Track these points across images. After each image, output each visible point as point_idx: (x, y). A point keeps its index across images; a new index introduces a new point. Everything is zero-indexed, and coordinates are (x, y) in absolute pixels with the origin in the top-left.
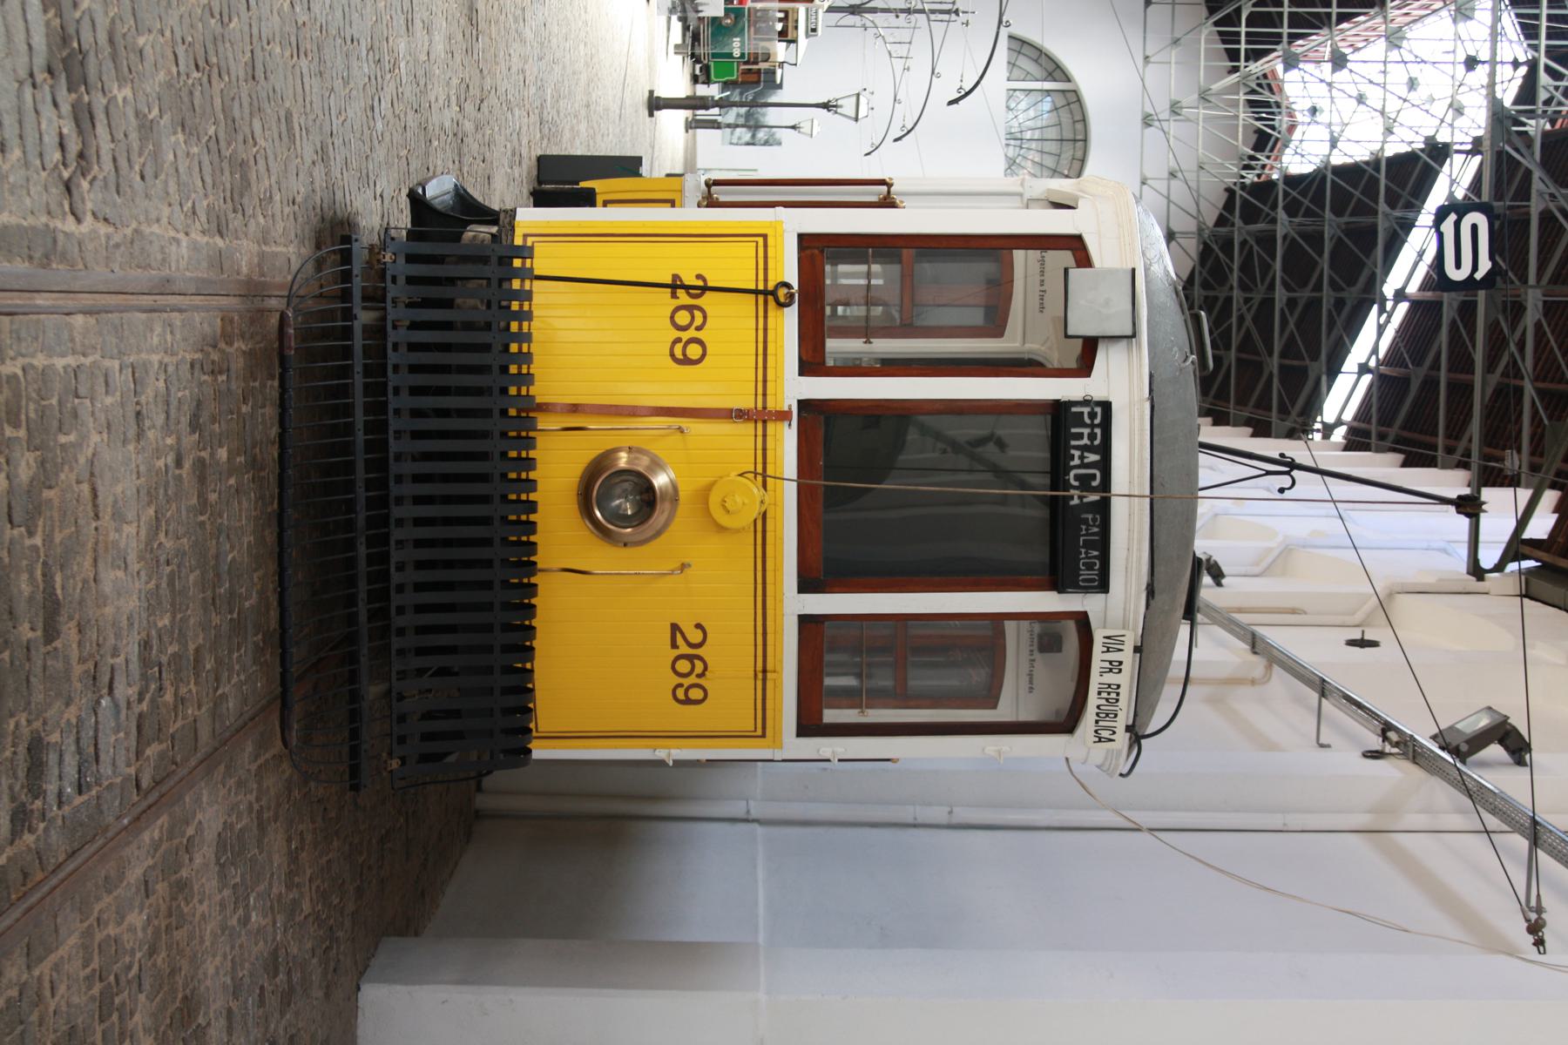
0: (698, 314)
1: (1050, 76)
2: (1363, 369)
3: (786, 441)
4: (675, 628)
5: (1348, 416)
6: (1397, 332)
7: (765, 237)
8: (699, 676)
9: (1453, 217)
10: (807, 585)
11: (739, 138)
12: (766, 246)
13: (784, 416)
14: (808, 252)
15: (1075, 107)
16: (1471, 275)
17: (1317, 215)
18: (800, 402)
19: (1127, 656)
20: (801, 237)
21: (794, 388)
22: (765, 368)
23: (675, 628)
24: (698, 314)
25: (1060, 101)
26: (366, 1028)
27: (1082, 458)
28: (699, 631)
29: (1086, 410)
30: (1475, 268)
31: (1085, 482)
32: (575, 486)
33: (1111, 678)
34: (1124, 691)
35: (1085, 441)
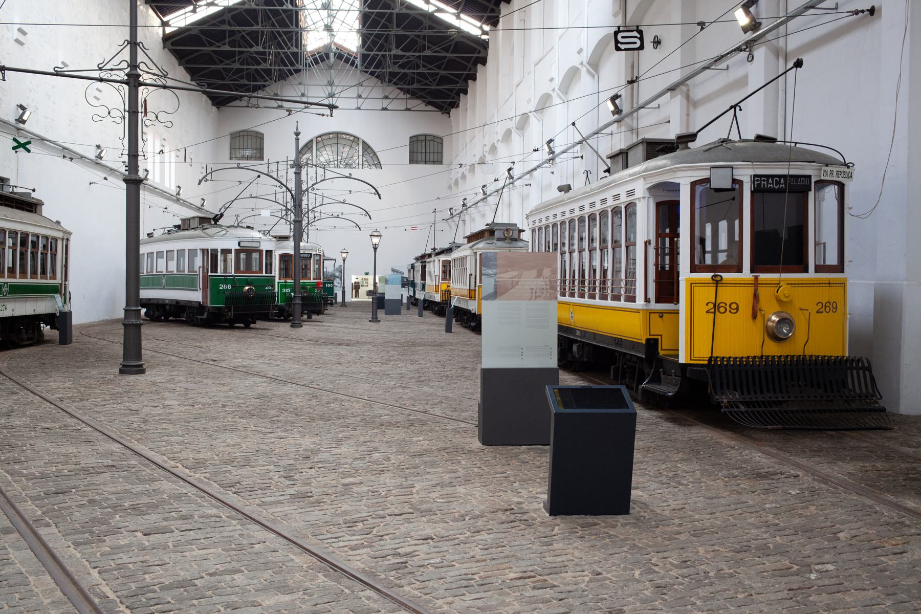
0: (721, 305)
1: (310, 149)
2: (458, 17)
3: (763, 276)
4: (818, 312)
5: (478, 24)
6: (448, 5)
7: (691, 284)
8: (726, 305)
9: (619, 45)
10: (806, 270)
11: (339, 283)
12: (695, 283)
13: (756, 278)
14: (697, 270)
15: (440, 154)
16: (639, 38)
17: (386, 36)
18: (751, 273)
19: (829, 169)
20: (691, 272)
21: (746, 274)
22: (740, 284)
23: (818, 312)
24: (721, 305)
25: (321, 145)
26: (913, 412)
27: (770, 184)
28: (709, 304)
29: (756, 183)
30: (636, 37)
31: (778, 183)
32: (773, 343)
33: (835, 174)
34: (838, 170)
35: (765, 183)
